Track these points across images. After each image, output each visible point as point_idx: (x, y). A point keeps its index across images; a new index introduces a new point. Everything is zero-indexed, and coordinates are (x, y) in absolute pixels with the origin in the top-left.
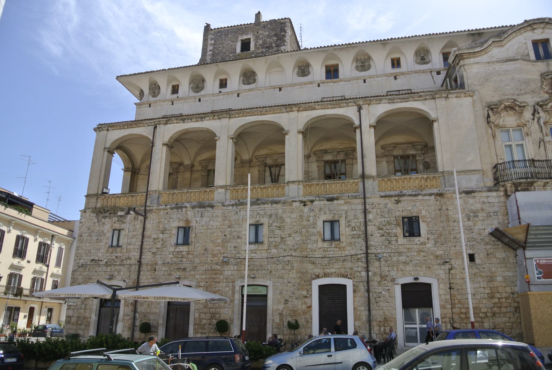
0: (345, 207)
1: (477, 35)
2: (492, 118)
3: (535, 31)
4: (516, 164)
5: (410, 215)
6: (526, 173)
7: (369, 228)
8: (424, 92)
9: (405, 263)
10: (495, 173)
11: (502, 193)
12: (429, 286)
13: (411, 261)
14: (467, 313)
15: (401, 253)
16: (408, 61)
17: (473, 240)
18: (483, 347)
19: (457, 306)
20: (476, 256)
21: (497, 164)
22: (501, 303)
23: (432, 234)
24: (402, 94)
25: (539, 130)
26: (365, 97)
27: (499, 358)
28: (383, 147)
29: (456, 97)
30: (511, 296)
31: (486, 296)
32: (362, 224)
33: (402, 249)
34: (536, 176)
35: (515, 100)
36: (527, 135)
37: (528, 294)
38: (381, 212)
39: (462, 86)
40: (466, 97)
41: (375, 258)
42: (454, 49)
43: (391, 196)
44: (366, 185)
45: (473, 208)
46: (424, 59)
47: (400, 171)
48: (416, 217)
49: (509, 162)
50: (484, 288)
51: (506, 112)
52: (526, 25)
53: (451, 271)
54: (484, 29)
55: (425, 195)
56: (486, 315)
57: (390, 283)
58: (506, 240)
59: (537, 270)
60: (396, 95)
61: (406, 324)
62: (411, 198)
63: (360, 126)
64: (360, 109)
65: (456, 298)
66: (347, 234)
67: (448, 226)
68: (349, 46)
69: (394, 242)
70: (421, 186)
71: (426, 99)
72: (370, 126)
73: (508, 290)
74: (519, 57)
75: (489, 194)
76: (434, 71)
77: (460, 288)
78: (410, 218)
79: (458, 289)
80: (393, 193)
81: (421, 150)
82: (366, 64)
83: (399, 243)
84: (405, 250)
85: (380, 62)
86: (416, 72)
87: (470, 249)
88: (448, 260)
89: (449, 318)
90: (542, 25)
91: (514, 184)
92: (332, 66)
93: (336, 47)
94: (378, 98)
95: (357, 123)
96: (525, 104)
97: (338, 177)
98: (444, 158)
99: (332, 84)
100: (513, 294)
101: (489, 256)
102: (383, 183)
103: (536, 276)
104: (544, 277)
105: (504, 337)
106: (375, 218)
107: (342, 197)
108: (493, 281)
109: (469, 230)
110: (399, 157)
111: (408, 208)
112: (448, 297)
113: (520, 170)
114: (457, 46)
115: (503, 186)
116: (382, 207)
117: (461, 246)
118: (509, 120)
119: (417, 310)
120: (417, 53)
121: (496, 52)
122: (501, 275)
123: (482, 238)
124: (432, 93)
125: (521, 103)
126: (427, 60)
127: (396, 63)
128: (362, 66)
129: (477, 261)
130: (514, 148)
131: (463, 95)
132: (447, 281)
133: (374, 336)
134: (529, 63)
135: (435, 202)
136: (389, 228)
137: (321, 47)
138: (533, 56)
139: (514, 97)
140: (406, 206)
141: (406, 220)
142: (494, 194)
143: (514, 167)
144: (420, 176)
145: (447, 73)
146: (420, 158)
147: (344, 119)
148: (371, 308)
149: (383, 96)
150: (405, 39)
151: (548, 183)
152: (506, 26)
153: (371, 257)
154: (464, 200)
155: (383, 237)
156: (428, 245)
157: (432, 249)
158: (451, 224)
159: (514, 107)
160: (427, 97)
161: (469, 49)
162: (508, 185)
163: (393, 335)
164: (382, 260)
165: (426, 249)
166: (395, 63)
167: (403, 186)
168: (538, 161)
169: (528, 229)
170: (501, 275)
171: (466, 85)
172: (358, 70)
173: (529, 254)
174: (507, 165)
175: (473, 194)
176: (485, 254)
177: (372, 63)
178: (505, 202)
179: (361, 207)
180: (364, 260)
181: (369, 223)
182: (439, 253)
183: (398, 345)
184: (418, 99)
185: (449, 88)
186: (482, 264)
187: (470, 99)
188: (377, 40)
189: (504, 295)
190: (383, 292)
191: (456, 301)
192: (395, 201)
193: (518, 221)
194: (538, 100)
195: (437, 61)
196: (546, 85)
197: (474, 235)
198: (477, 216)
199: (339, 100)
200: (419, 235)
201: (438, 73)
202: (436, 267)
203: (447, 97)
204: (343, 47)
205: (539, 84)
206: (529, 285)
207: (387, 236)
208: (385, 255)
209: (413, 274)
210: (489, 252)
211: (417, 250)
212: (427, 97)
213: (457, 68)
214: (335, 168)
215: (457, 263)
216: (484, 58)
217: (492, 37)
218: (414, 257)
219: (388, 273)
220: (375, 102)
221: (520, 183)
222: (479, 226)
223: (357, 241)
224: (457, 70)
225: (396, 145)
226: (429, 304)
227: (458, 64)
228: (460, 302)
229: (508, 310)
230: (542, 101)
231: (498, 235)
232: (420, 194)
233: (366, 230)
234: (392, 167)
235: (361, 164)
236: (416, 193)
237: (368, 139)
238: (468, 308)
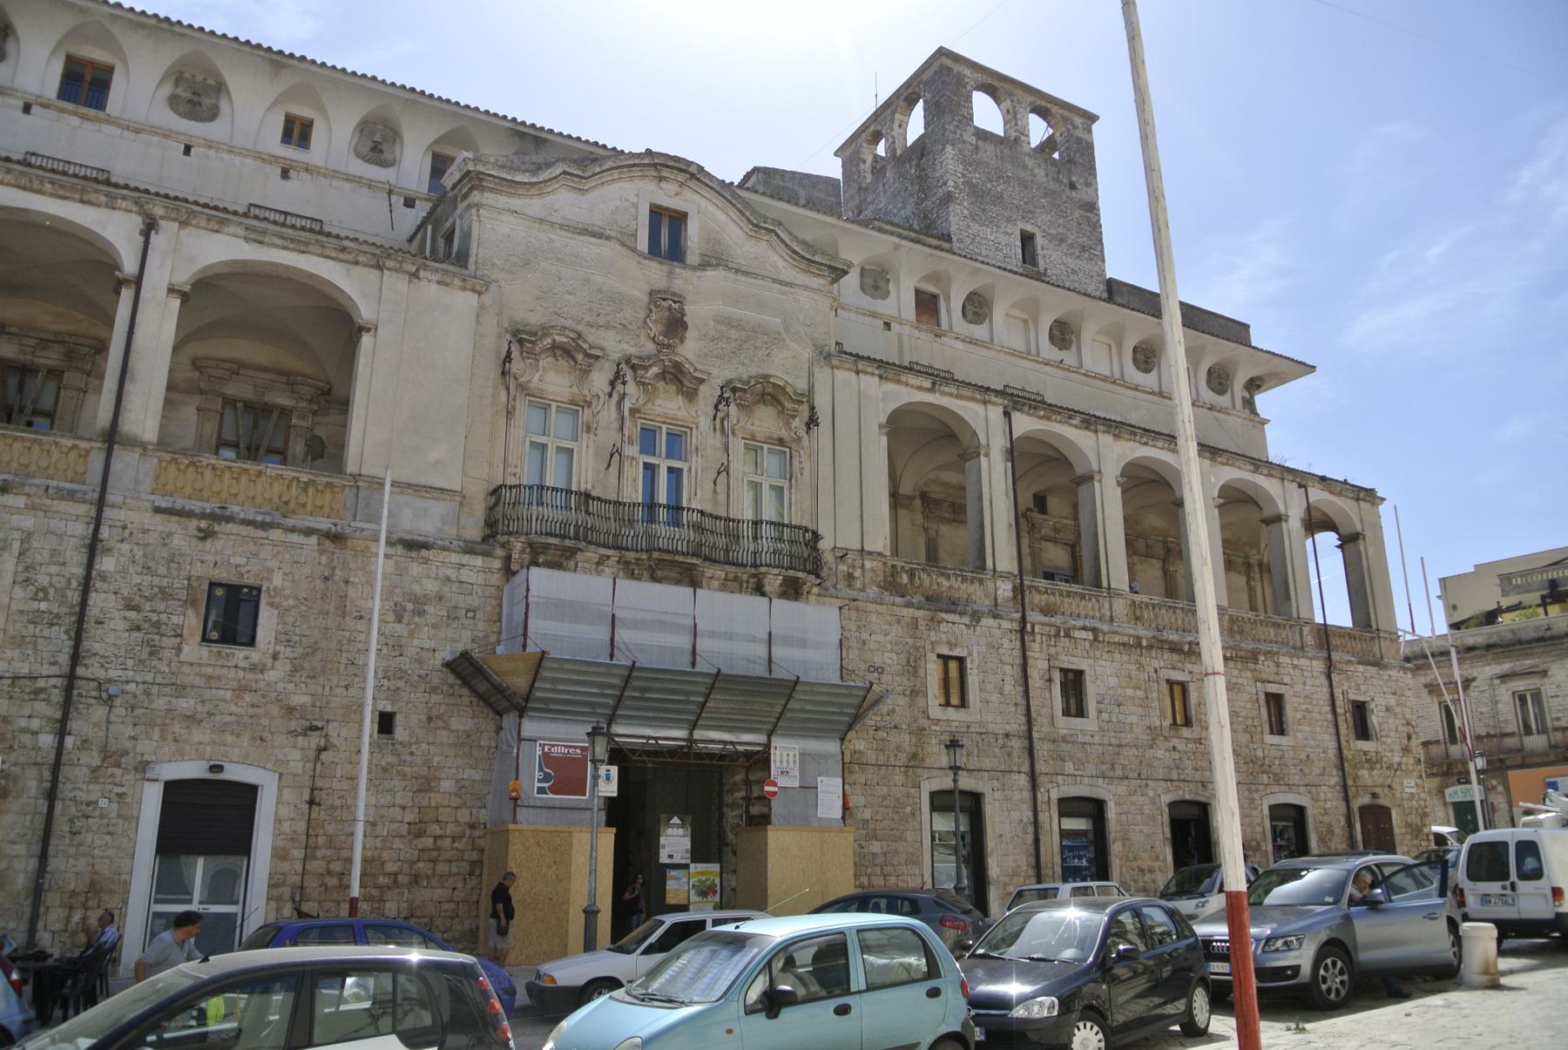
0: (28, 522)
1: (531, 141)
2: (516, 366)
3: (664, 184)
4: (547, 496)
5: (235, 580)
6: (565, 524)
7: (95, 599)
8: (356, 239)
9: (192, 719)
10: (491, 509)
11: (497, 564)
12: (251, 791)
13: (210, 714)
14: (345, 874)
15: (184, 687)
16: (335, 138)
17: (399, 674)
18: (362, 968)
19: (319, 854)
20: (399, 720)
21: (500, 487)
22: (439, 850)
23: (289, 643)
24: (293, 227)
25: (616, 425)
26: (176, 198)
27: (400, 996)
28: (196, 364)
29: (439, 283)
30: (468, 832)
31: (404, 829)
32: (74, 584)
33: (190, 677)
34: (585, 536)
35: (580, 336)
36: (588, 430)
37: (508, 831)
38: (145, 555)
39: (462, 259)
40: (464, 289)
41: (94, 694)
42: (465, 154)
43: (190, 514)
44: (116, 465)
45: (416, 588)
46: (381, 151)
47: (235, 446)
48: (251, 588)
49: (531, 487)
50: (404, 808)
51: (551, 359)
52: (646, 161)
53: (324, 756)
54: (551, 131)
55: (293, 530)
56: (395, 881)
57: (131, 777)
58: (483, 687)
59: (541, 769)
60: (275, 223)
61: (157, 901)
62: (249, 530)
63: (138, 281)
64: (149, 228)
65: (321, 832)
66: (14, 607)
67: (340, 628)
68: (165, 26)
69: (167, 654)
70: (287, 503)
71: (356, 263)
72: (171, 290)
73: (464, 816)
74: (613, 234)
75: (466, 559)
76: (398, 194)
77: (338, 803)
78: (233, 590)
79: (333, 807)
80: (196, 506)
81: (310, 401)
82: (206, 101)
83: (183, 657)
84: (197, 682)
85: (252, 112)
86: (349, 178)
87: (387, 699)
88: (320, 724)
89: (293, 886)
90: (681, 177)
91: (531, 545)
92: (93, 64)
93: (118, 12)
94: (217, 215)
95: (130, 267)
96: (600, 353)
97: (24, 419)
98: (368, 436)
99: (75, 121)
100: (472, 826)
101: (433, 725)
102: (172, 469)
103: (537, 785)
104: (553, 790)
105: (427, 941)
106: (124, 572)
107: (23, 485)
108: (430, 790)
109: (393, 646)
110: (240, 405)
111: (231, 556)
112: (302, 826)
113: (552, 513)
114: (475, 149)
115: (503, 546)
116: (152, 541)
117: (364, 689)
118: (555, 381)
119: (201, 861)
120: (365, 127)
121: (564, 202)
122: (455, 773)
123: (423, 673)
124: (378, 252)
125: (591, 347)
126: (387, 156)
127: (297, 132)
128: (190, 101)
129: (400, 733)
130: (551, 451)
131: (457, 282)
132: (306, 781)
133: (45, 939)
134: (631, 254)
135: (317, 554)
136: (162, 608)
137: (374, 78)
138: (643, 244)
139: (580, 328)
140: (228, 552)
141: (219, 592)
142: (479, 561)
143: (540, 503)
144: (289, 473)
145: (433, 210)
146: (301, 423)
147: (89, 243)
148: (51, 850)
149: (235, 213)
150: (341, 76)
151: (608, 557)
152: (604, 146)
153: (84, 689)
154: (396, 562)
155: (135, 634)
156: (272, 675)
157: (281, 685)
158: (349, 622)
159: (574, 353)
160: (361, 258)
161: (502, 167)
162: (518, 545)
163: (110, 933)
164: (118, 702)
165: (261, 685)
166: (297, 130)
167: (233, 491)
168: (599, 499)
169: (539, 666)
170: (455, 773)
171: (472, 260)
172: (175, 111)
173: (530, 727)
174: (525, 495)
175: (424, 552)
176: (424, 718)
177: (224, 105)
178: (500, 589)
179: (81, 529)
180: (57, 696)
181: (98, 584)
182: (300, 699)
183: (121, 968)
184: (333, 254)
185: (428, 253)
186: (410, 744)
187: (473, 299)
188: (259, 46)
189: (451, 829)
190: (103, 803)
191: (321, 840)
192: (199, 530)
193: (521, 639)
194: (632, 351)
195: (412, 169)
196: (655, 322)
197: (405, 664)
198: (421, 613)
199: (85, 178)
200: (251, 642)
201: (409, 203)
202: (282, 739)
203: (415, 275)
204: (142, 19)
205: (642, 316)
206: (516, 806)
207: (151, 635)
208: (131, 687)
209: (208, 755)
210: (434, 713)
211: (235, 684)
212: (361, 258)
213: (461, 207)
214: (21, 388)
215: (343, 734)
216: (534, 205)
217: (564, 159)
218: (222, 705)
219: (128, 745)
220: (203, 223)
221: (547, 546)
222: (423, 639)
223: (46, 632)
224: (459, 211)
225: (238, 368)
226: (243, 846)
227: (465, 196)
228: (330, 843)
229: (454, 870)
230: (639, 358)
231: (465, 669)
232: (279, 526)
233: (84, 603)
234: (211, 428)
235: (113, 397)
236: (268, 519)
237: (154, 330)
238: (350, 860)
